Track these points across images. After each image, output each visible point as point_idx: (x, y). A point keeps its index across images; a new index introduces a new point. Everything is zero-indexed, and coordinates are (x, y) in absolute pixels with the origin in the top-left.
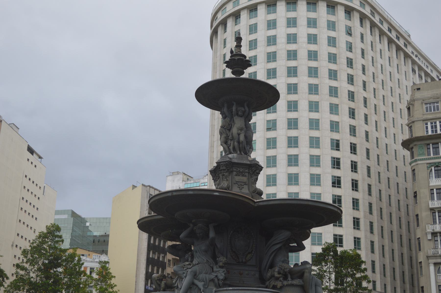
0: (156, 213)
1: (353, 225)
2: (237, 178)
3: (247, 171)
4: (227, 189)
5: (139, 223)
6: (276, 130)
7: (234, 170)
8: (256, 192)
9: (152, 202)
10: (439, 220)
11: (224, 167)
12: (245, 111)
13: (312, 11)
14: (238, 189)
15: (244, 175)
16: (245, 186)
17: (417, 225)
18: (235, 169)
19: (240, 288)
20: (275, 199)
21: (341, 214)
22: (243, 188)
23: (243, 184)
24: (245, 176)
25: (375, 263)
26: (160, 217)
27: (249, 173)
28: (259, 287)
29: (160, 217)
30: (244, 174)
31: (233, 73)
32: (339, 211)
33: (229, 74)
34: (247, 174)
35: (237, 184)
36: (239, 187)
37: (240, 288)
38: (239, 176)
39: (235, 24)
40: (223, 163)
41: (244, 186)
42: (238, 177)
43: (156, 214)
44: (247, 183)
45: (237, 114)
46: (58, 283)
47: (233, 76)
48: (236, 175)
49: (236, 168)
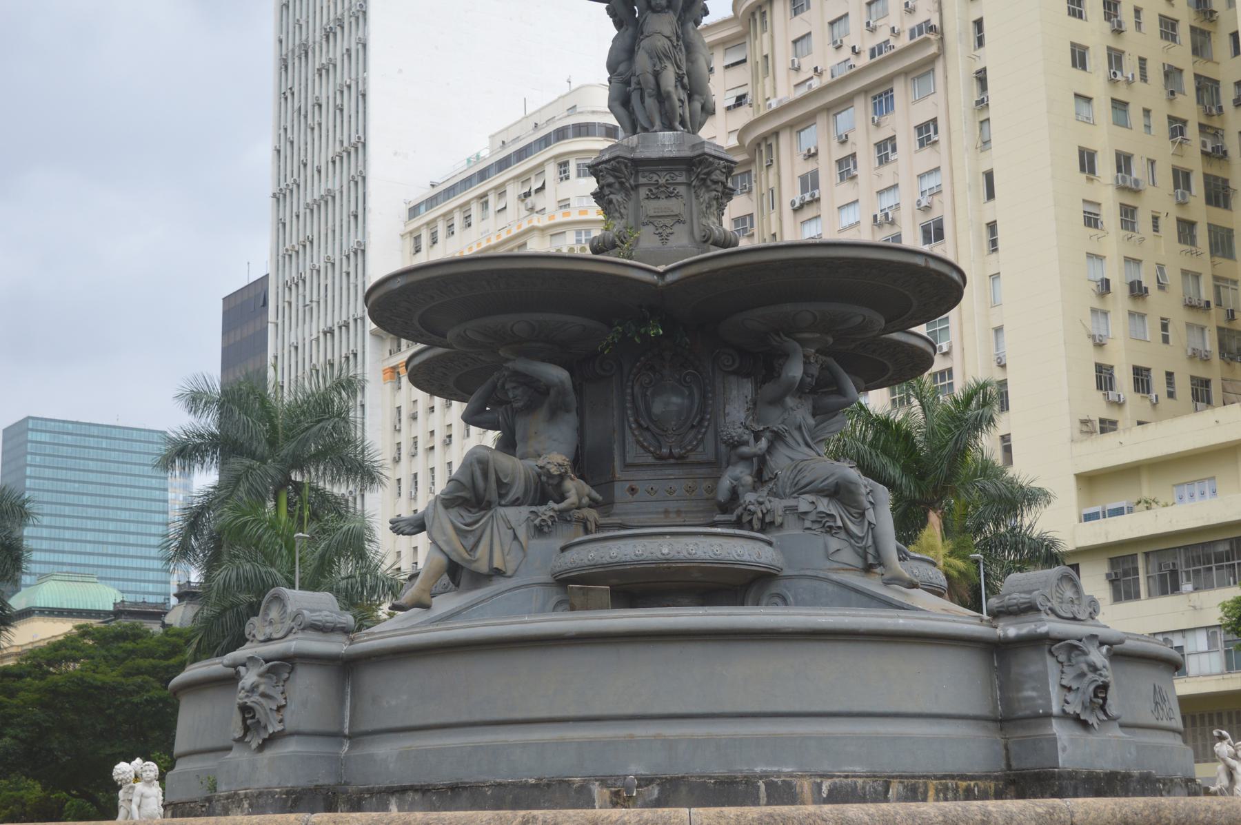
0: (421, 343)
2: (652, 207)
3: (682, 179)
4: (618, 243)
5: (409, 368)
6: (1112, 367)
7: (640, 182)
8: (710, 241)
11: (607, 176)
13: (950, 381)
14: (657, 237)
15: (672, 193)
16: (677, 228)
18: (643, 177)
19: (719, 530)
21: (962, 284)
22: (671, 234)
23: (669, 222)
24: (677, 196)
26: (439, 351)
27: (689, 185)
29: (439, 351)
30: (674, 189)
32: (955, 276)
34: (682, 190)
35: (651, 226)
36: (657, 232)
37: (719, 530)
39: (877, 155)
40: (604, 165)
41: (673, 228)
43: (422, 346)
44: (685, 217)
46: (637, 340)
49: (647, 174)
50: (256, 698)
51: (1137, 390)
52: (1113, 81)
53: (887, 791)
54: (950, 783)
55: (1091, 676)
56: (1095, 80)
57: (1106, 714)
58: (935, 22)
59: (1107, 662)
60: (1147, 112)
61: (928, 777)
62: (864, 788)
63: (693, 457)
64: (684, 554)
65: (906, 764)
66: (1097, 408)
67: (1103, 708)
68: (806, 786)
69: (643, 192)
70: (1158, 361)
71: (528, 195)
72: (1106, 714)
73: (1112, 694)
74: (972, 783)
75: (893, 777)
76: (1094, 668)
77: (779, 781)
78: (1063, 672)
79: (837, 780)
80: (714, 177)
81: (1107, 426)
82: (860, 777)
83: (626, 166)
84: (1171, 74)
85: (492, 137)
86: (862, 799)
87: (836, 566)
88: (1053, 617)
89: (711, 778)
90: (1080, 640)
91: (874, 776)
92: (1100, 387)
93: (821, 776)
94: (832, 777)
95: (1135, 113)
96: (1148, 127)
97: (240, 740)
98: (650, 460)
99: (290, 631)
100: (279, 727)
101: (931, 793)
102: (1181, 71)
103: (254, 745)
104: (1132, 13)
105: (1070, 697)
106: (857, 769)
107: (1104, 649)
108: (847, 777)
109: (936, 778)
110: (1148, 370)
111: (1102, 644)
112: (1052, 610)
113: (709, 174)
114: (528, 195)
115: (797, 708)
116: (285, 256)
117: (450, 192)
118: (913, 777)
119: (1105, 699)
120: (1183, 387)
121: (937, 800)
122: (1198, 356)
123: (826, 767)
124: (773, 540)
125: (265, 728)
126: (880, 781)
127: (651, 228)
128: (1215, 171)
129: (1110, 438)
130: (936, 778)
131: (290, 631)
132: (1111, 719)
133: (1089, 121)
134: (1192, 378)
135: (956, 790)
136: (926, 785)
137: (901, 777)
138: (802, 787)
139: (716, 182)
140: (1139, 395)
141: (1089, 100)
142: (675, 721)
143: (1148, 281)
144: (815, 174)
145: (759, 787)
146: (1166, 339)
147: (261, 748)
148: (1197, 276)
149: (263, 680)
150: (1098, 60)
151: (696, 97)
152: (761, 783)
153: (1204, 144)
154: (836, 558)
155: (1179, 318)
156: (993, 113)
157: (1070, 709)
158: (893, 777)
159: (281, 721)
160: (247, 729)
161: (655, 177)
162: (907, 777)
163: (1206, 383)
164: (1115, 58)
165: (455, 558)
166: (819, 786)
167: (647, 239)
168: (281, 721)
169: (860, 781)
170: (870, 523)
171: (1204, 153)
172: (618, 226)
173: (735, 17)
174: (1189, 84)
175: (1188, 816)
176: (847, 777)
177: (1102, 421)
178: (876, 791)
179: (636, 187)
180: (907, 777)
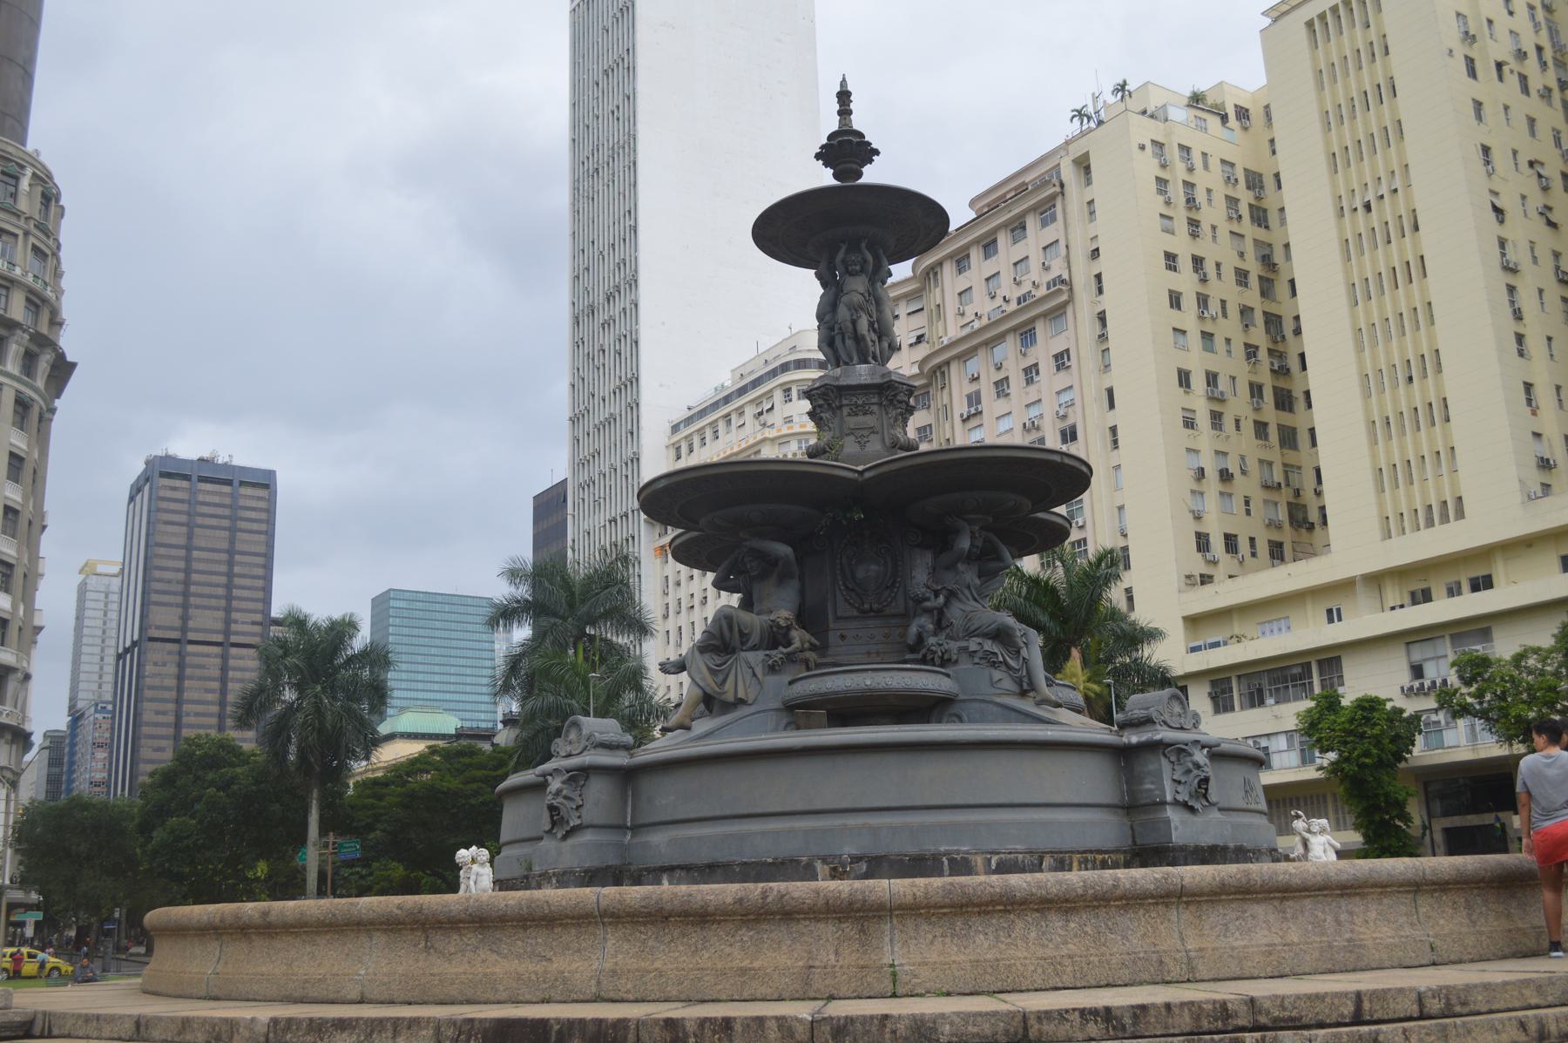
1: (1363, 572)
2: (852, 422)
9: (644, 498)
10: (56, 1032)
12: (865, 261)
17: (181, 1000)
20: (916, 452)
23: (865, 433)
24: (871, 413)
25: (1088, 1006)
26: (695, 534)
27: (880, 404)
28: (905, 662)
29: (695, 534)
31: (836, 176)
32: (1084, 469)
33: (825, 177)
34: (875, 408)
38: (857, 415)
42: (855, 418)
43: (680, 531)
45: (851, 274)
47: (835, 182)
48: (849, 415)
50: (560, 799)
51: (1227, 551)
52: (1201, 318)
53: (1041, 864)
54: (1089, 856)
55: (1195, 772)
56: (1188, 317)
57: (1208, 801)
58: (1065, 276)
59: (1207, 761)
60: (1228, 341)
61: (1072, 852)
62: (1023, 861)
63: (888, 611)
64: (882, 685)
65: (1056, 842)
66: (1198, 566)
67: (1205, 796)
68: (979, 861)
69: (846, 411)
70: (1244, 528)
71: (761, 414)
72: (1208, 801)
73: (1213, 787)
74: (1107, 856)
75: (1046, 853)
76: (1198, 766)
77: (958, 857)
78: (1174, 770)
79: (1003, 856)
80: (899, 398)
81: (1206, 579)
82: (1021, 853)
83: (832, 391)
84: (1245, 311)
85: (733, 371)
86: (1023, 870)
87: (998, 691)
88: (1165, 728)
89: (906, 856)
90: (1187, 745)
91: (1031, 852)
92: (1199, 550)
93: (991, 853)
94: (999, 853)
95: (1219, 342)
96: (1229, 352)
97: (549, 832)
98: (855, 613)
99: (585, 749)
100: (578, 822)
101: (1075, 864)
102: (1252, 309)
103: (559, 835)
104: (1214, 267)
105: (1180, 788)
106: (1018, 847)
107: (1205, 751)
108: (1010, 853)
109: (1079, 852)
110: (1236, 536)
111: (1203, 747)
112: (1165, 723)
113: (895, 396)
114: (761, 414)
115: (971, 801)
116: (579, 464)
117: (702, 413)
118: (1061, 852)
119: (1206, 789)
120: (1263, 549)
121: (1080, 870)
122: (1273, 525)
123: (994, 846)
124: (951, 673)
125: (568, 822)
126: (1036, 856)
127: (852, 438)
128: (1281, 384)
129: (1208, 588)
130: (1079, 852)
131: (585, 749)
132: (1212, 804)
133: (1185, 348)
134: (1269, 541)
135: (1094, 861)
136: (1071, 858)
137: (1052, 852)
138: (976, 861)
139: (900, 402)
140: (1229, 556)
141: (1184, 332)
142: (798, 816)
143: (1234, 468)
144: (978, 393)
145: (943, 863)
146: (1248, 512)
147: (564, 838)
148: (1270, 464)
149: (565, 786)
150: (1189, 302)
151: (884, 338)
152: (944, 859)
153: (1272, 364)
154: (999, 685)
155: (1258, 496)
156: (1112, 343)
157: (1180, 798)
158: (1046, 853)
159: (579, 817)
160: (554, 823)
161: (855, 399)
162: (1056, 853)
163: (1280, 545)
164: (1203, 301)
165: (709, 691)
166: (989, 860)
167: (850, 446)
168: (579, 817)
169: (1020, 856)
170: (1024, 659)
171: (1273, 371)
172: (827, 436)
173: (914, 277)
174: (1259, 318)
175: (1271, 878)
176: (1010, 853)
177: (1202, 576)
178: (1033, 864)
179: (840, 407)
180: (1056, 853)
